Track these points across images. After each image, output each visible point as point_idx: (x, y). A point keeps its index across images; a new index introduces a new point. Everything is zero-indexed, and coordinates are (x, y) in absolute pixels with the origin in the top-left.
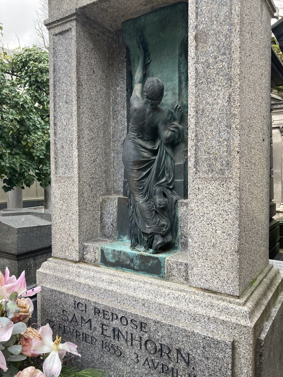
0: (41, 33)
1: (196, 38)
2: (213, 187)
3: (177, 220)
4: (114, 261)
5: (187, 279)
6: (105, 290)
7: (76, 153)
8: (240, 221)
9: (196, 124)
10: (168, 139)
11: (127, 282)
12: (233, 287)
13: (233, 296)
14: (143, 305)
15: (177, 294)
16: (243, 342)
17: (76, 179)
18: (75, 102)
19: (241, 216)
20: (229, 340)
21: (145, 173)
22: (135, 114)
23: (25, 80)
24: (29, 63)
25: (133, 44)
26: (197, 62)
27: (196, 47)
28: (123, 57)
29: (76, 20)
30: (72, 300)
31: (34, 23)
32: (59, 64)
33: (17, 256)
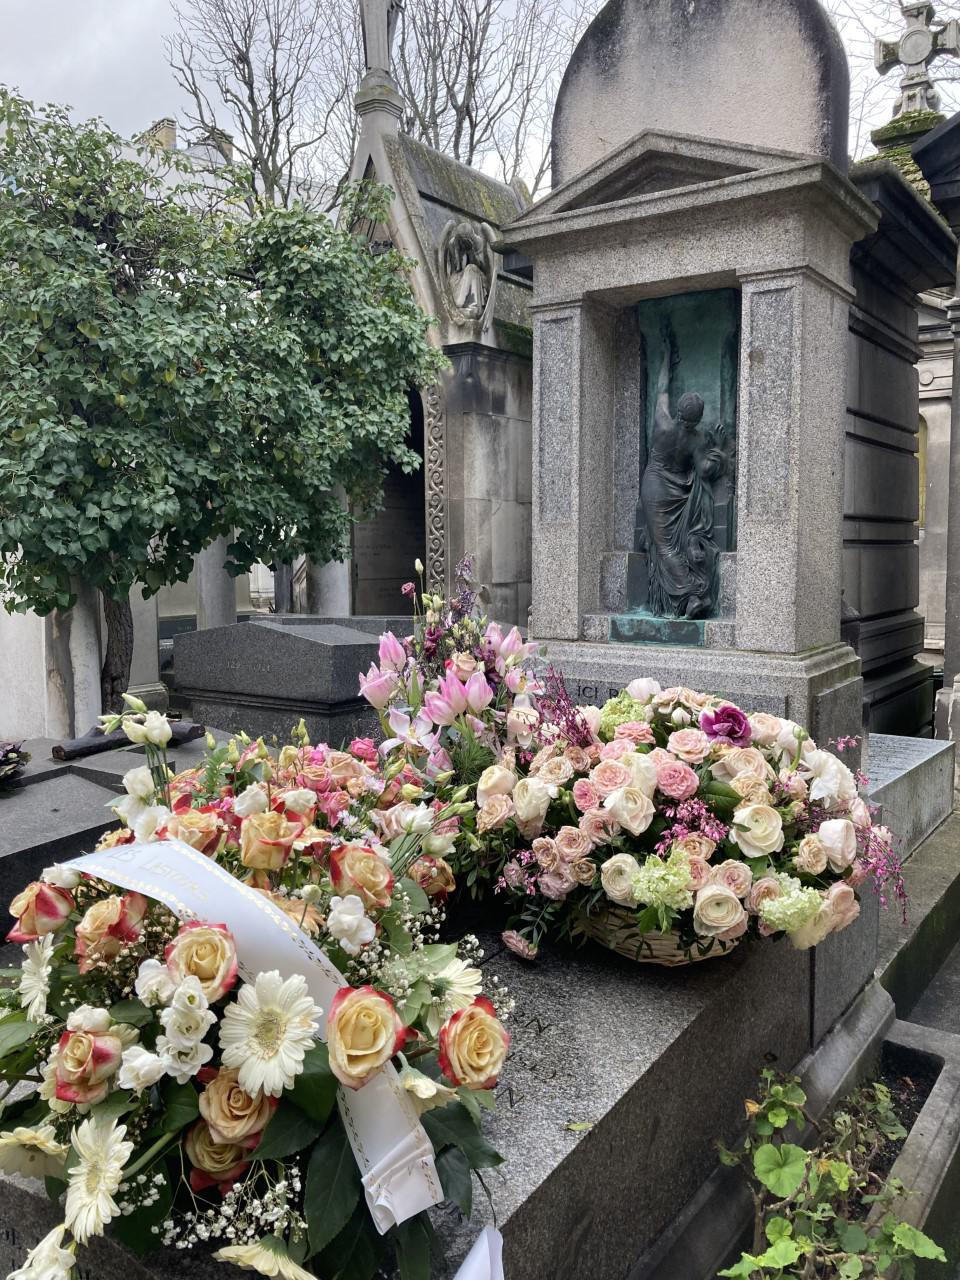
0: (191, 81)
1: (751, 356)
2: (766, 531)
3: (719, 579)
4: (632, 633)
5: (733, 644)
6: (624, 666)
7: (575, 491)
8: (798, 569)
9: (750, 456)
10: (706, 472)
11: (655, 654)
12: (789, 644)
13: (788, 653)
14: (679, 676)
15: (721, 659)
16: (798, 695)
17: (575, 527)
18: (577, 420)
19: (798, 565)
20: (782, 696)
21: (673, 518)
22: (663, 438)
23: (275, 292)
24: (289, 248)
25: (653, 333)
26: (751, 385)
27: (751, 367)
28: (636, 350)
29: (581, 307)
30: (574, 686)
31: (168, 44)
32: (550, 363)
33: (331, 705)
